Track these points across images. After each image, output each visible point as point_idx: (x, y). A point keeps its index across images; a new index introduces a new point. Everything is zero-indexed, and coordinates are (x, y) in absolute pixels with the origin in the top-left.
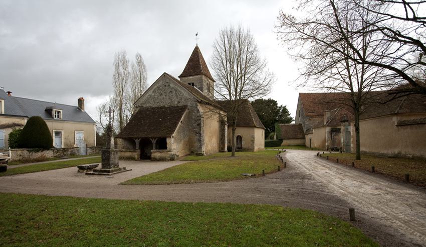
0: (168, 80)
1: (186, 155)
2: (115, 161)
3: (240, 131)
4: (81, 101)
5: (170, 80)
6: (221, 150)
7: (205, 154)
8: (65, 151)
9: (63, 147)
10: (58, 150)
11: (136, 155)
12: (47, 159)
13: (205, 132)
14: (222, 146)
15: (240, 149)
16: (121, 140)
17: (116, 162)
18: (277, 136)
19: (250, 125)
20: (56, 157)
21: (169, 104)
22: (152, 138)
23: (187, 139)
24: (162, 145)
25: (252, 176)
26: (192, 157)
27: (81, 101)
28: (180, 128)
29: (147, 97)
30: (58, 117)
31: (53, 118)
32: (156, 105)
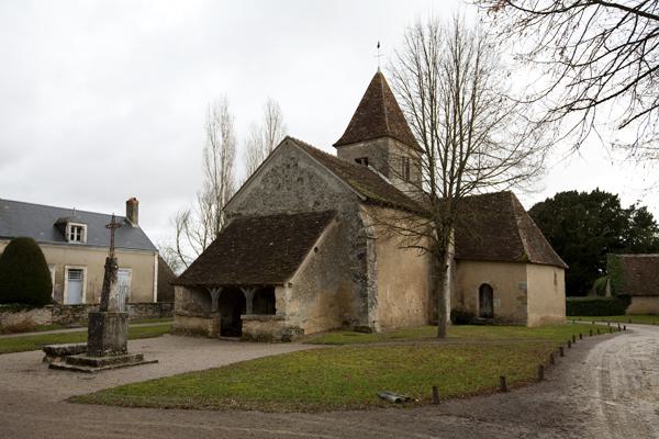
1: (330, 330)
2: (116, 341)
4: (132, 205)
5: (298, 152)
6: (434, 318)
7: (378, 330)
8: (78, 311)
9: (84, 301)
10: (64, 309)
11: (210, 325)
12: (36, 328)
13: (381, 275)
15: (489, 319)
16: (181, 289)
17: (121, 340)
18: (612, 286)
19: (511, 256)
20: (58, 323)
21: (296, 209)
22: (242, 285)
23: (332, 291)
24: (266, 302)
25: (398, 401)
26: (341, 336)
27: (132, 205)
28: (311, 265)
30: (78, 238)
32: (266, 211)
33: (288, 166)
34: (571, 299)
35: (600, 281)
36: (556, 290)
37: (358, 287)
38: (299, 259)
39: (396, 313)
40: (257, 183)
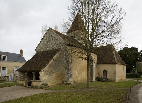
0: (51, 33)
1: (58, 84)
3: (104, 67)
4: (21, 51)
7: (72, 84)
11: (24, 83)
14: (91, 77)
15: (106, 80)
18: (137, 70)
19: (112, 62)
27: (21, 51)
28: (52, 64)
29: (41, 45)
30: (5, 59)
31: (2, 60)
33: (50, 36)
34: (127, 73)
35: (134, 69)
36: (124, 71)
37: (66, 71)
38: (47, 62)
39: (79, 78)
40: (42, 42)
